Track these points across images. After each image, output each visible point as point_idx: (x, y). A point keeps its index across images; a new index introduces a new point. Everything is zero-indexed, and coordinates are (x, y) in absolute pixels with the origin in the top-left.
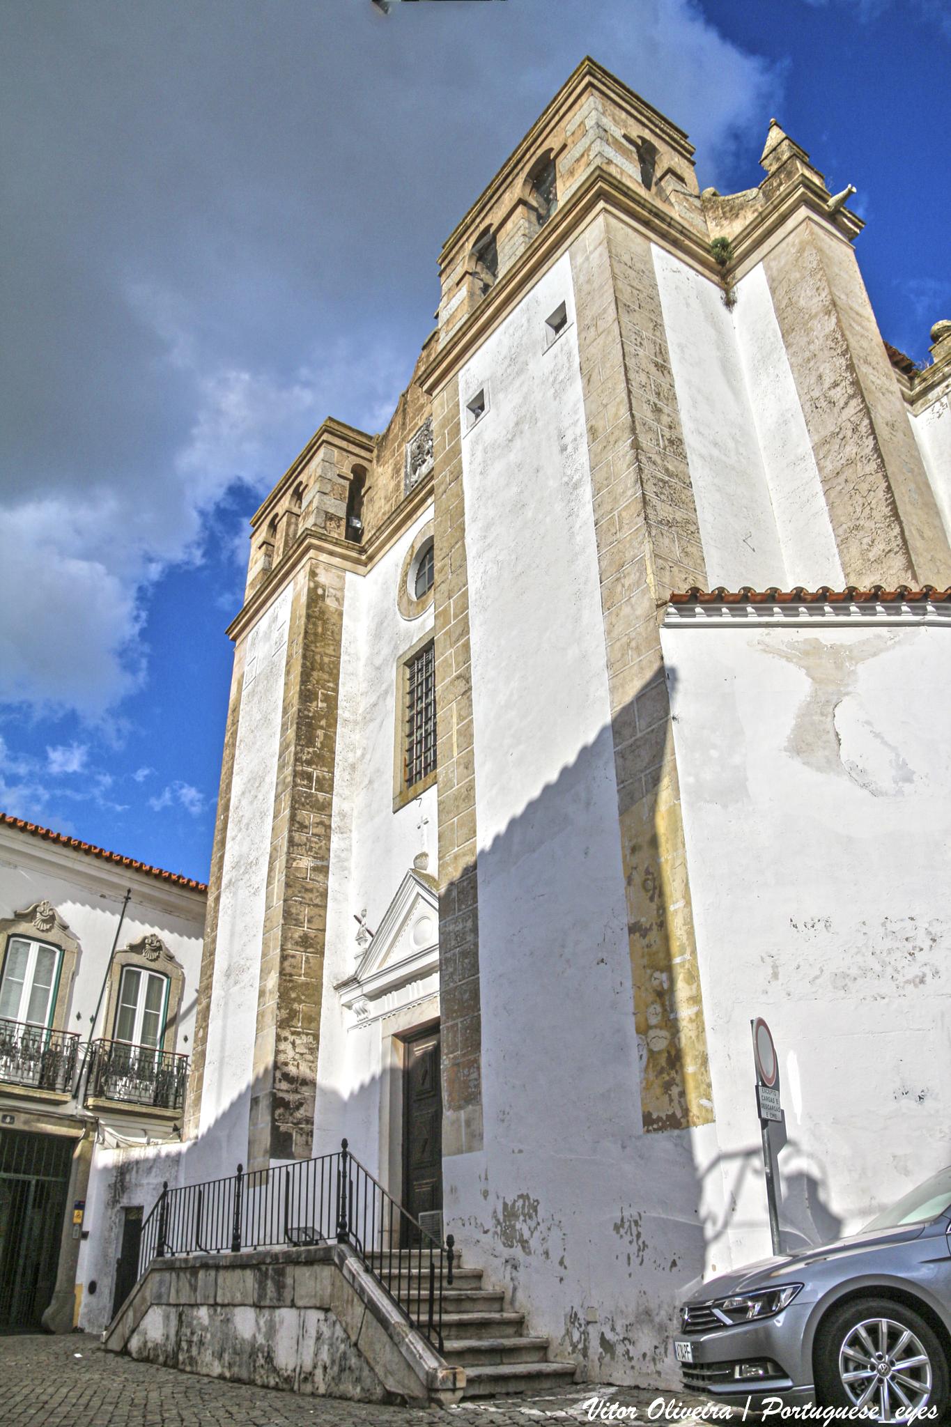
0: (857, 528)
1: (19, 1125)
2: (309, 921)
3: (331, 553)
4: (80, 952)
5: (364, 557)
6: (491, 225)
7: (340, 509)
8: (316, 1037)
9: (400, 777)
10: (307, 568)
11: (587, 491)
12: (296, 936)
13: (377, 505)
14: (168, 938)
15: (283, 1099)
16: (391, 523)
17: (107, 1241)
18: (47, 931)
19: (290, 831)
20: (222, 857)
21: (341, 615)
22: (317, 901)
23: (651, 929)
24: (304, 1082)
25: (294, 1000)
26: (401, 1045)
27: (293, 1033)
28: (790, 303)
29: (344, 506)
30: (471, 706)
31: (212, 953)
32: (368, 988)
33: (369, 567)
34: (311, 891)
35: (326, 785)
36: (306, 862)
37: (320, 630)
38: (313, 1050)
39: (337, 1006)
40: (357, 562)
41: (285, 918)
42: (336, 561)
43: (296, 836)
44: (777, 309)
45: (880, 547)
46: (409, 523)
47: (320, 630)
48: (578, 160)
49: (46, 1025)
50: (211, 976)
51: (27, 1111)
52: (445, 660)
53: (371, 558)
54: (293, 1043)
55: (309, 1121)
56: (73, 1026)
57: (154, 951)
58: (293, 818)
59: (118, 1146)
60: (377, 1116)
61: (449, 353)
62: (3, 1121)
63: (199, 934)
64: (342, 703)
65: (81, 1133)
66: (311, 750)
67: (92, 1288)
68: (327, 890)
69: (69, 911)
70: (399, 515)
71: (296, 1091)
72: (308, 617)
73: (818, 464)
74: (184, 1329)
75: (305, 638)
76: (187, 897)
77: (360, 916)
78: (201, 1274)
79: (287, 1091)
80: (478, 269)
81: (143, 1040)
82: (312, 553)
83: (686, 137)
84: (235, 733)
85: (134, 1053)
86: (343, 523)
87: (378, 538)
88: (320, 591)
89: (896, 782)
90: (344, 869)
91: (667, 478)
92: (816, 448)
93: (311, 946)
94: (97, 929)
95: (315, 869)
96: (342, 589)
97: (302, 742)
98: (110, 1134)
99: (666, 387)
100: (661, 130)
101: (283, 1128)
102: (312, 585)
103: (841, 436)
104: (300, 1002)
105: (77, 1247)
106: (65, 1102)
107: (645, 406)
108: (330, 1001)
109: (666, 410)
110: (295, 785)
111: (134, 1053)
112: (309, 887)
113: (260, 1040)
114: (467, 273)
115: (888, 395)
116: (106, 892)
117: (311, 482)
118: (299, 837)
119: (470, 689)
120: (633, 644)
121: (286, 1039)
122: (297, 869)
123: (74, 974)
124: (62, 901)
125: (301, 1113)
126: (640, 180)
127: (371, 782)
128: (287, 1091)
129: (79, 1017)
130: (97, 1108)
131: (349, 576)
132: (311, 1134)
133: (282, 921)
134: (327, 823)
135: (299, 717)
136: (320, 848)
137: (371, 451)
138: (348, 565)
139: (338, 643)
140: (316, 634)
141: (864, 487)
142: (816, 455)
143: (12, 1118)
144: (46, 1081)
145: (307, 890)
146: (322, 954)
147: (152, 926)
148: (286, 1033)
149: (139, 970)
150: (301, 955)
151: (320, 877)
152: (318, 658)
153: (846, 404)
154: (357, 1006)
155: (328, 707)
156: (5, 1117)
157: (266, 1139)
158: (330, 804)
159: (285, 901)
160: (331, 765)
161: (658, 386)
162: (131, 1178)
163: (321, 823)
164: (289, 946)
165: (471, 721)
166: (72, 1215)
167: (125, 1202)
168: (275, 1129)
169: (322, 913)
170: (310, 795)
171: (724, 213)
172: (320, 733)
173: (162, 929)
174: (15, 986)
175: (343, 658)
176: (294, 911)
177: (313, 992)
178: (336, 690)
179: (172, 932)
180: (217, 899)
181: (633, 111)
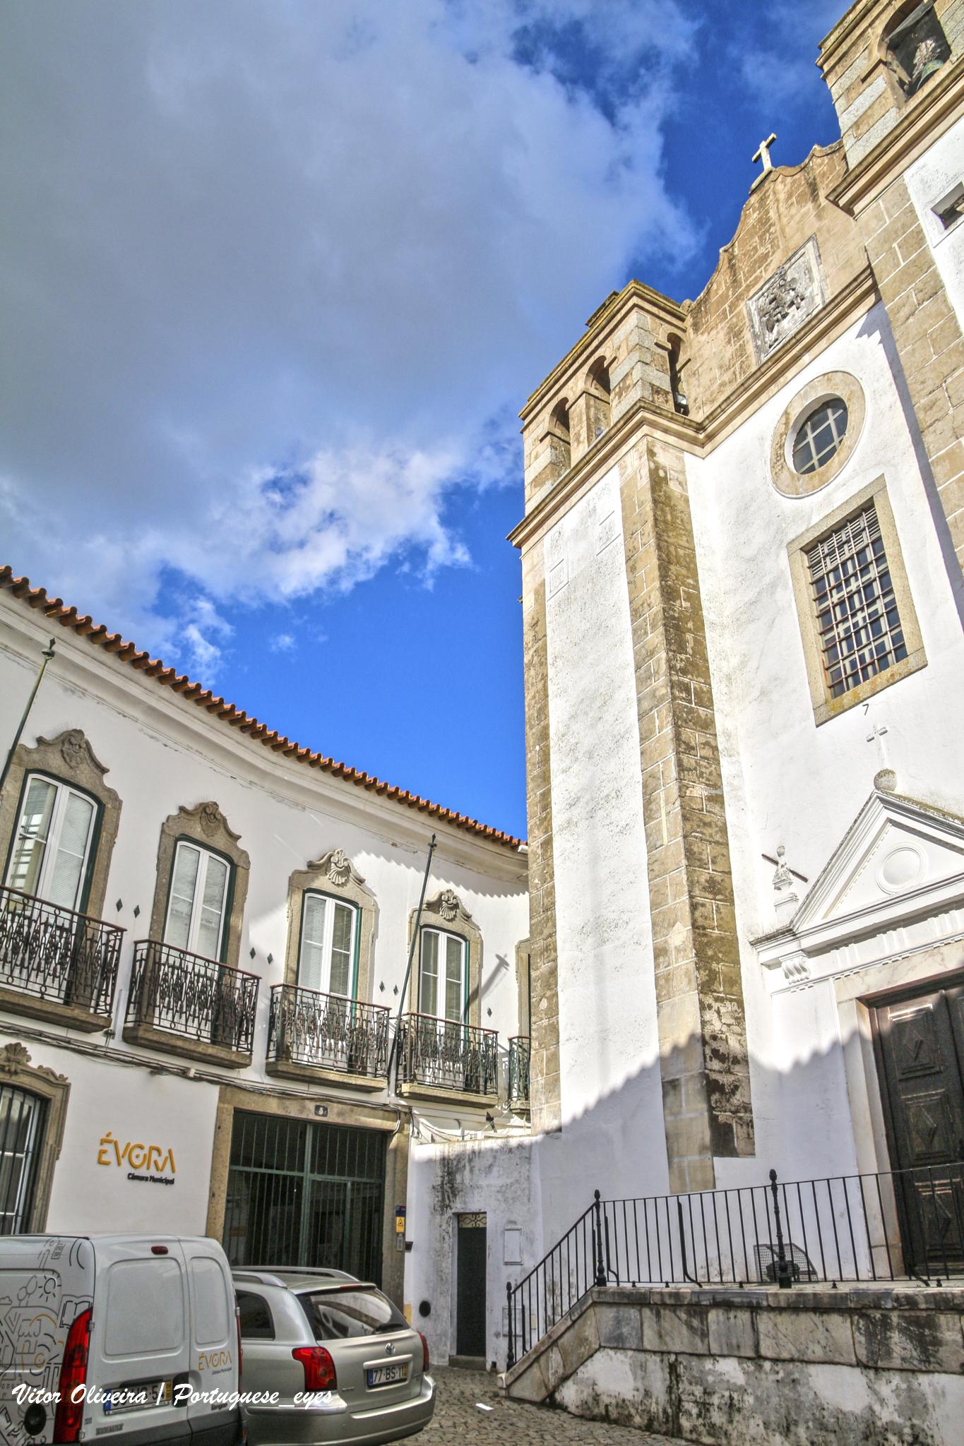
1: (333, 1117)
3: (666, 431)
4: (377, 911)
5: (701, 436)
7: (664, 382)
8: (740, 1004)
9: (822, 682)
10: (643, 447)
12: (703, 879)
13: (705, 379)
14: (462, 893)
15: (716, 1081)
16: (746, 390)
17: (439, 1253)
18: (343, 885)
19: (678, 753)
20: (546, 796)
21: (687, 501)
22: (718, 838)
24: (736, 1061)
25: (711, 958)
26: (865, 1010)
27: (717, 999)
31: (550, 908)
32: (808, 942)
33: (708, 447)
35: (705, 699)
36: (699, 791)
37: (669, 517)
38: (740, 1020)
39: (757, 966)
40: (694, 441)
41: (688, 858)
42: (672, 439)
43: (684, 757)
46: (773, 388)
47: (669, 517)
49: (349, 996)
51: (340, 1101)
53: (710, 437)
54: (718, 1012)
55: (747, 1108)
56: (378, 998)
57: (451, 909)
58: (678, 737)
59: (433, 1140)
60: (844, 1098)
61: (885, 151)
62: (317, 1114)
63: (520, 884)
64: (705, 604)
65: (395, 1125)
66: (683, 656)
67: (425, 1309)
68: (725, 824)
69: (364, 863)
70: (758, 379)
71: (729, 1071)
72: (655, 501)
74: (684, 1386)
75: (656, 525)
76: (498, 845)
77: (773, 855)
78: (713, 1315)
79: (720, 1072)
80: (889, 58)
81: (448, 1014)
82: (645, 429)
84: (542, 652)
85: (441, 1028)
87: (723, 411)
88: (662, 474)
90: (739, 799)
93: (719, 892)
94: (394, 885)
95: (710, 799)
96: (683, 472)
97: (674, 648)
98: (425, 1127)
101: (723, 1117)
102: (652, 465)
104: (718, 961)
105: (402, 1260)
106: (381, 1089)
108: (750, 960)
110: (674, 698)
111: (441, 1028)
112: (707, 820)
113: (666, 1010)
114: (880, 61)
116: (398, 840)
117: (622, 354)
118: (688, 760)
121: (710, 1007)
122: (692, 798)
123: (374, 936)
124: (356, 852)
125: (737, 1099)
127: (763, 693)
128: (720, 1072)
129: (382, 988)
130: (414, 1096)
132: (750, 1124)
133: (684, 862)
134: (713, 744)
135: (665, 618)
136: (711, 773)
137: (683, 320)
138: (684, 445)
139: (689, 533)
140: (665, 522)
143: (325, 1109)
144: (354, 1065)
145: (705, 824)
146: (732, 902)
147: (447, 881)
148: (709, 1000)
149: (439, 928)
150: (710, 904)
151: (717, 809)
152: (672, 549)
154: (789, 964)
155: (692, 607)
156: (317, 1108)
157: (703, 1132)
159: (685, 837)
160: (705, 673)
162: (464, 1178)
163: (707, 744)
164: (697, 892)
166: (394, 1222)
167: (458, 1206)
168: (713, 1119)
169: (724, 851)
170: (691, 711)
172: (689, 636)
173: (458, 885)
174: (313, 951)
175: (698, 551)
176: (696, 849)
177: (729, 947)
178: (696, 587)
179: (467, 889)
180: (547, 844)
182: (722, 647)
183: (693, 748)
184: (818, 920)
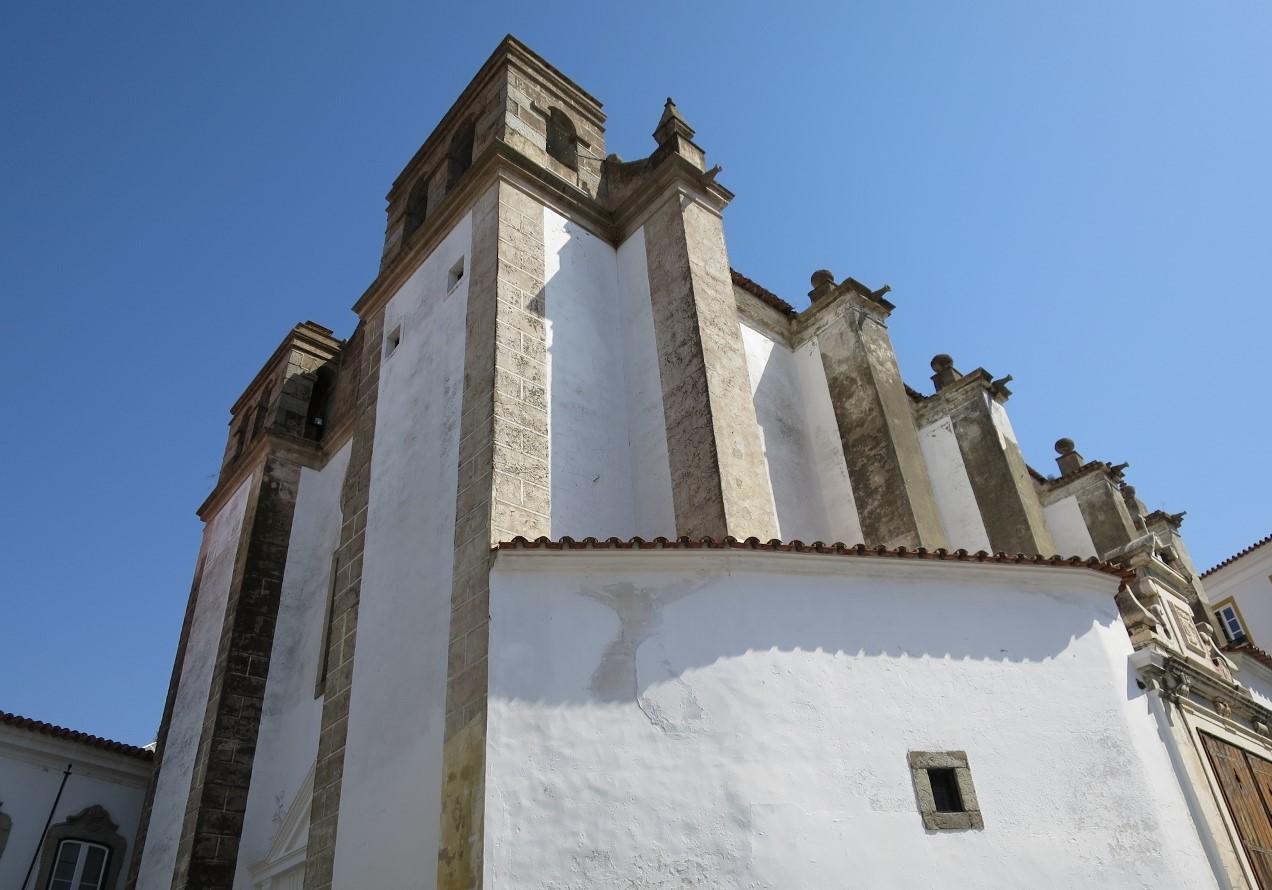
0: (688, 474)
2: (228, 804)
6: (426, 173)
11: (457, 433)
19: (219, 715)
21: (293, 506)
23: (453, 858)
28: (660, 266)
29: (306, 405)
30: (356, 618)
34: (233, 773)
35: (262, 670)
36: (232, 745)
44: (650, 270)
45: (702, 495)
48: (490, 128)
50: (141, 852)
52: (345, 571)
73: (665, 413)
83: (600, 105)
86: (304, 421)
88: (274, 485)
89: (685, 718)
91: (522, 427)
92: (665, 399)
96: (296, 483)
99: (536, 340)
100: (576, 101)
102: (266, 479)
103: (684, 390)
107: (510, 360)
109: (533, 362)
115: (730, 354)
119: (358, 603)
120: (471, 583)
122: (222, 752)
126: (543, 146)
131: (305, 470)
134: (258, 705)
136: (248, 731)
139: (287, 533)
141: (696, 438)
142: (665, 405)
153: (690, 361)
158: (262, 688)
161: (528, 340)
163: (252, 706)
165: (355, 633)
171: (621, 177)
181: (549, 85)
182: (507, 453)
183: (236, 710)
184: (282, 854)
